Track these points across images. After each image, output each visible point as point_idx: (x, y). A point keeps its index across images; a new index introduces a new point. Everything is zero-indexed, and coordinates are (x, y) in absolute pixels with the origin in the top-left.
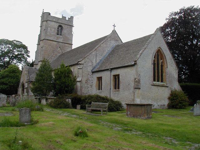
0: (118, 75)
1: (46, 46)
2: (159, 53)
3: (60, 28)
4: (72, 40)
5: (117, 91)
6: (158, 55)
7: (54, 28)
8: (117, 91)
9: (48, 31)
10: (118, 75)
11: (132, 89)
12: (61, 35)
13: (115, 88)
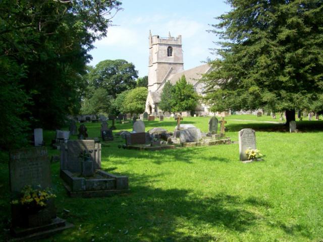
4: (182, 59)
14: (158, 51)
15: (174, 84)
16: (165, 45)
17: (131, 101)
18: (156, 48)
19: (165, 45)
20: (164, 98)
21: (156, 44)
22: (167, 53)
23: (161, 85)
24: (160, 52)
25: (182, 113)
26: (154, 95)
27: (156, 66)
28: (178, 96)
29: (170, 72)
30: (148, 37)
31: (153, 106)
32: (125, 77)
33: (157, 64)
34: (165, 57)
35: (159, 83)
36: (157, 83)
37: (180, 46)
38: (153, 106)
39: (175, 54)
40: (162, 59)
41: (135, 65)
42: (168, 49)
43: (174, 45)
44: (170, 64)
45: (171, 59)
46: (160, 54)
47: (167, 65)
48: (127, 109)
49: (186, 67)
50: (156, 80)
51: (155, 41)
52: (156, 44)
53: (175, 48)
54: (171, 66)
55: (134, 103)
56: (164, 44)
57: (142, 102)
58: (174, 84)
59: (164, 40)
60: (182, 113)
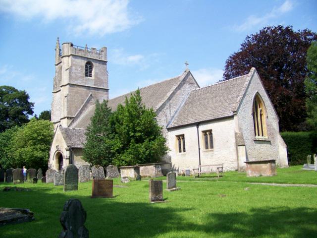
0: (210, 131)
1: (71, 94)
2: (257, 100)
3: (89, 66)
4: (107, 83)
5: (210, 151)
6: (256, 102)
7: (81, 67)
8: (210, 151)
9: (73, 71)
10: (210, 131)
11: (233, 147)
12: (91, 76)
13: (207, 148)
14: (71, 67)
15: (114, 108)
16: (82, 57)
17: (22, 143)
18: (67, 62)
19: (82, 57)
20: (93, 135)
21: (69, 56)
22: (84, 71)
23: (73, 122)
24: (74, 68)
25: (141, 168)
26: (67, 134)
27: (65, 91)
28: (128, 131)
29: (88, 102)
30: (55, 47)
31: (66, 154)
32: (12, 112)
33: (68, 86)
34: (81, 77)
35: (71, 118)
36: (68, 118)
37: (105, 63)
38: (66, 154)
39: (96, 73)
40: (76, 79)
41: (30, 95)
42: (86, 66)
43: (96, 61)
44: (89, 88)
45: (91, 82)
46: (74, 71)
47: (84, 90)
48: (308, 180)
49: (112, 95)
50: (66, 112)
51: (67, 50)
52: (69, 56)
53: (97, 64)
54: (90, 92)
55: (28, 149)
56: (82, 57)
57: (43, 147)
58: (114, 108)
59: (80, 50)
60: (141, 168)
